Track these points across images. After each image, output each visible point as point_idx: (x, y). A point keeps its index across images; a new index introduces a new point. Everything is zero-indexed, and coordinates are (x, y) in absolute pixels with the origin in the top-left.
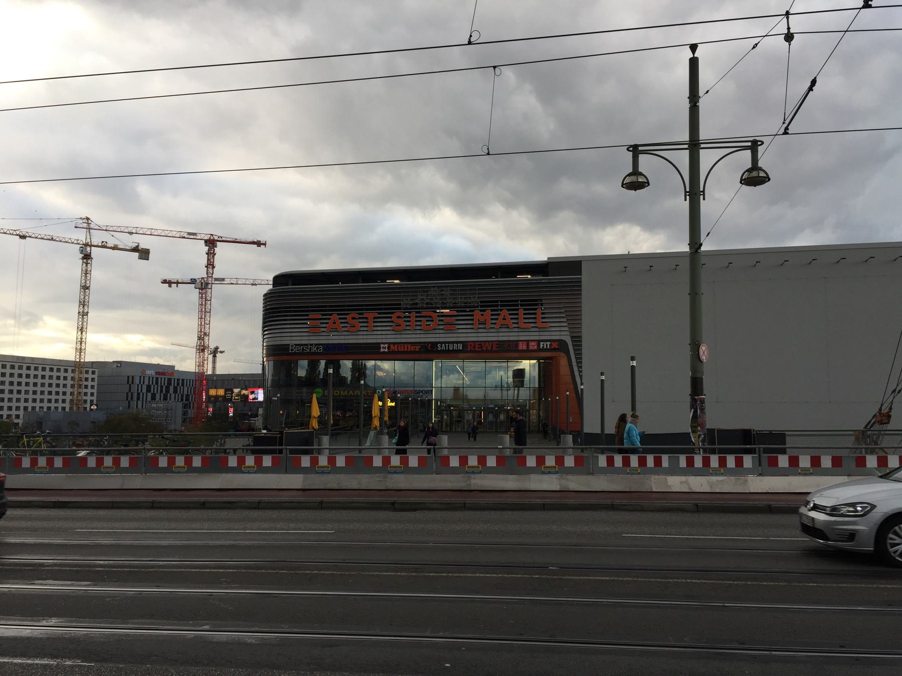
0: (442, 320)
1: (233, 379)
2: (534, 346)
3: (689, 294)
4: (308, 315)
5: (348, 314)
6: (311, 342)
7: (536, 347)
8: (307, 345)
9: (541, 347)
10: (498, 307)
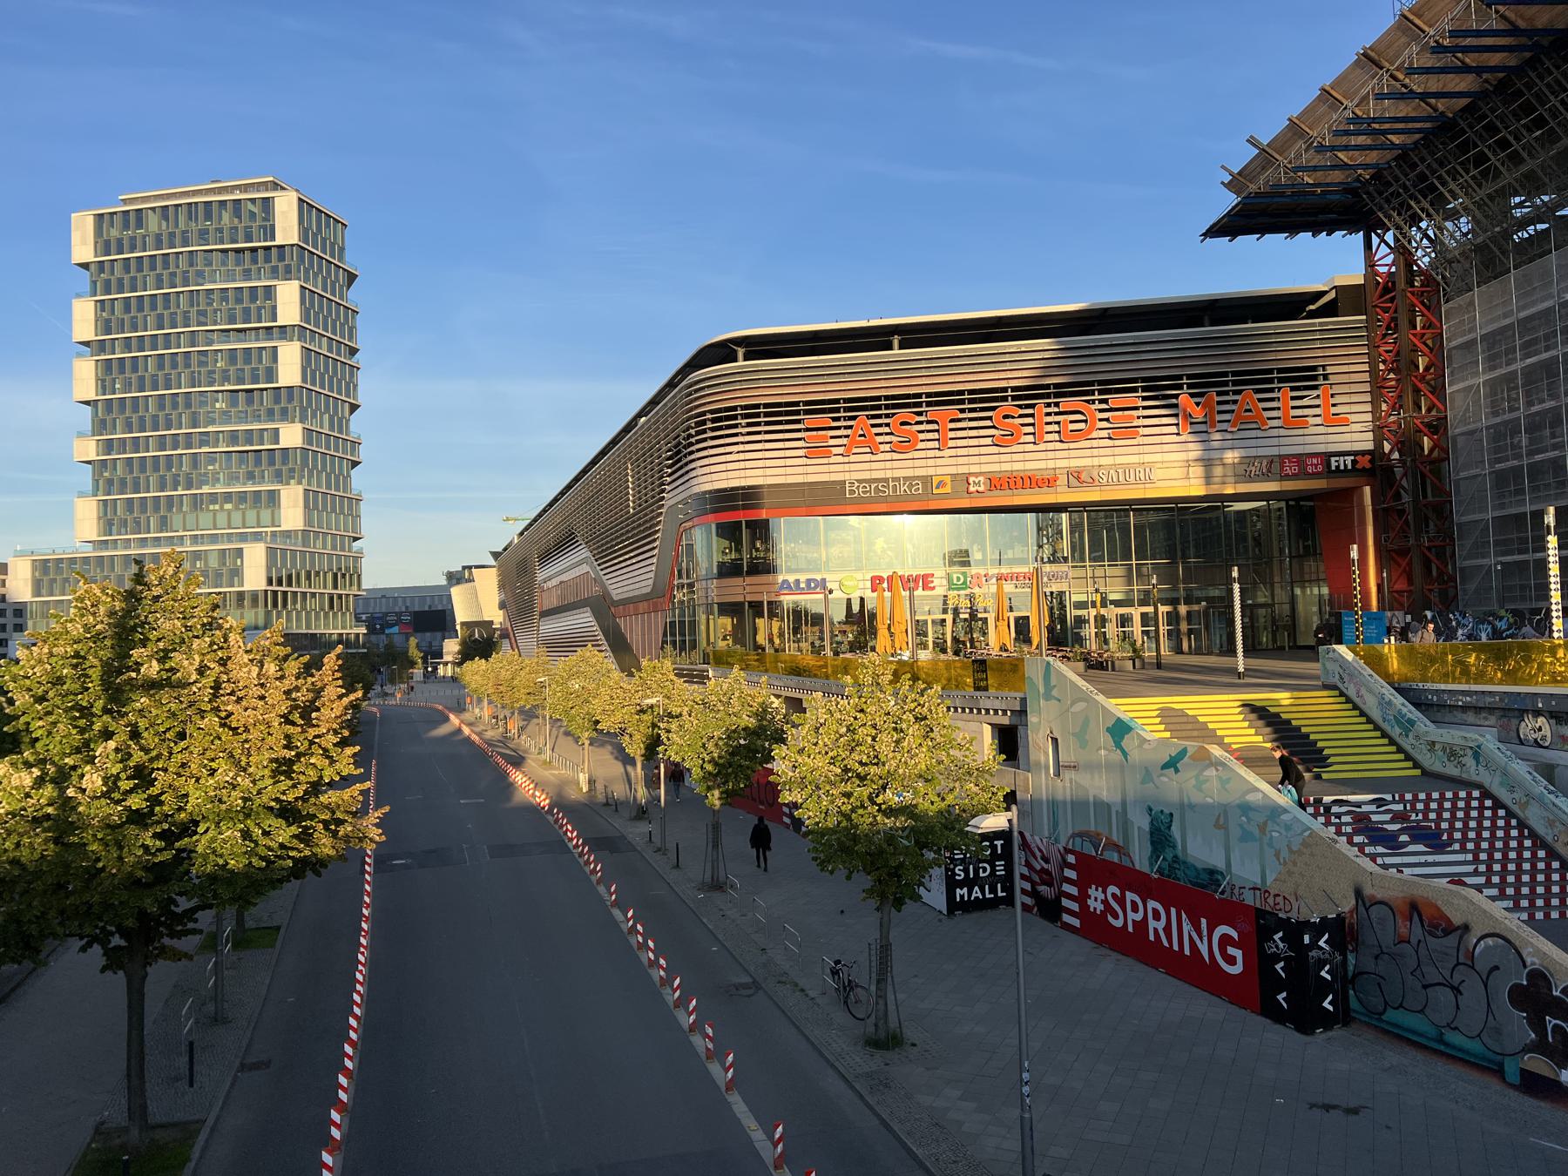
0: (1107, 420)
1: (384, 596)
2: (1316, 465)
3: (354, 408)
4: (798, 422)
5: (993, 409)
6: (897, 474)
7: (1320, 468)
8: (886, 480)
9: (1333, 468)
10: (1273, 383)
